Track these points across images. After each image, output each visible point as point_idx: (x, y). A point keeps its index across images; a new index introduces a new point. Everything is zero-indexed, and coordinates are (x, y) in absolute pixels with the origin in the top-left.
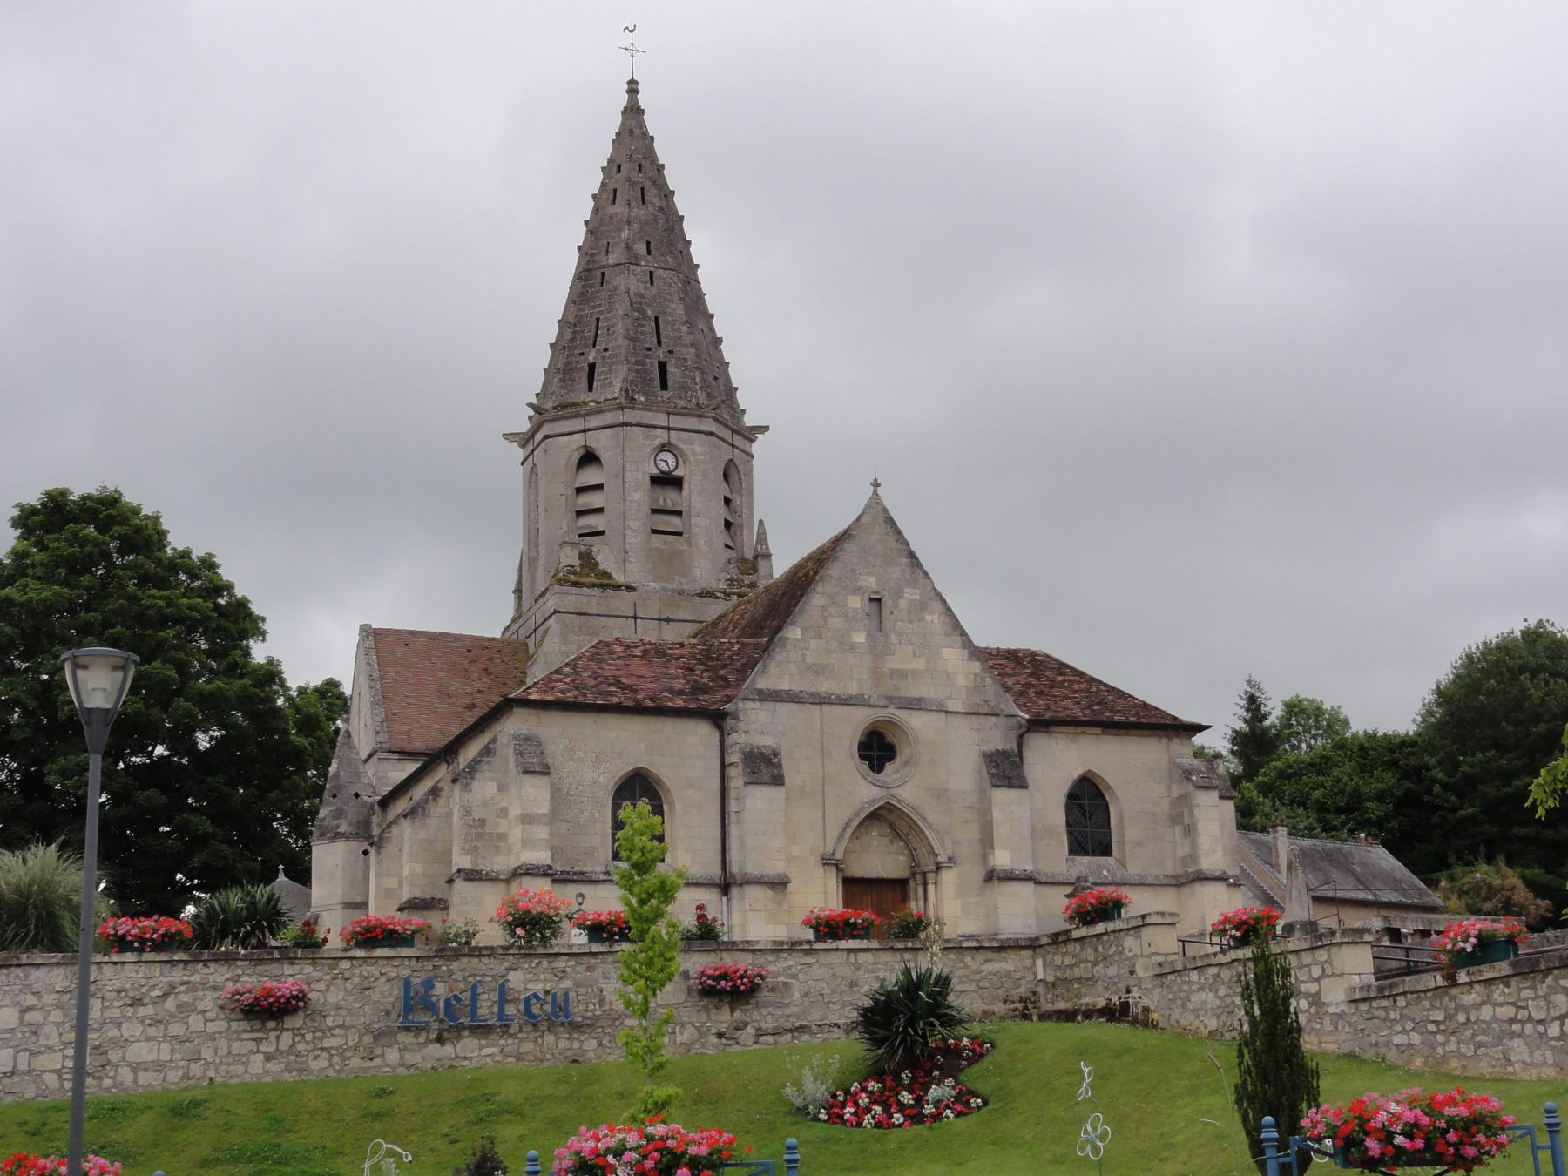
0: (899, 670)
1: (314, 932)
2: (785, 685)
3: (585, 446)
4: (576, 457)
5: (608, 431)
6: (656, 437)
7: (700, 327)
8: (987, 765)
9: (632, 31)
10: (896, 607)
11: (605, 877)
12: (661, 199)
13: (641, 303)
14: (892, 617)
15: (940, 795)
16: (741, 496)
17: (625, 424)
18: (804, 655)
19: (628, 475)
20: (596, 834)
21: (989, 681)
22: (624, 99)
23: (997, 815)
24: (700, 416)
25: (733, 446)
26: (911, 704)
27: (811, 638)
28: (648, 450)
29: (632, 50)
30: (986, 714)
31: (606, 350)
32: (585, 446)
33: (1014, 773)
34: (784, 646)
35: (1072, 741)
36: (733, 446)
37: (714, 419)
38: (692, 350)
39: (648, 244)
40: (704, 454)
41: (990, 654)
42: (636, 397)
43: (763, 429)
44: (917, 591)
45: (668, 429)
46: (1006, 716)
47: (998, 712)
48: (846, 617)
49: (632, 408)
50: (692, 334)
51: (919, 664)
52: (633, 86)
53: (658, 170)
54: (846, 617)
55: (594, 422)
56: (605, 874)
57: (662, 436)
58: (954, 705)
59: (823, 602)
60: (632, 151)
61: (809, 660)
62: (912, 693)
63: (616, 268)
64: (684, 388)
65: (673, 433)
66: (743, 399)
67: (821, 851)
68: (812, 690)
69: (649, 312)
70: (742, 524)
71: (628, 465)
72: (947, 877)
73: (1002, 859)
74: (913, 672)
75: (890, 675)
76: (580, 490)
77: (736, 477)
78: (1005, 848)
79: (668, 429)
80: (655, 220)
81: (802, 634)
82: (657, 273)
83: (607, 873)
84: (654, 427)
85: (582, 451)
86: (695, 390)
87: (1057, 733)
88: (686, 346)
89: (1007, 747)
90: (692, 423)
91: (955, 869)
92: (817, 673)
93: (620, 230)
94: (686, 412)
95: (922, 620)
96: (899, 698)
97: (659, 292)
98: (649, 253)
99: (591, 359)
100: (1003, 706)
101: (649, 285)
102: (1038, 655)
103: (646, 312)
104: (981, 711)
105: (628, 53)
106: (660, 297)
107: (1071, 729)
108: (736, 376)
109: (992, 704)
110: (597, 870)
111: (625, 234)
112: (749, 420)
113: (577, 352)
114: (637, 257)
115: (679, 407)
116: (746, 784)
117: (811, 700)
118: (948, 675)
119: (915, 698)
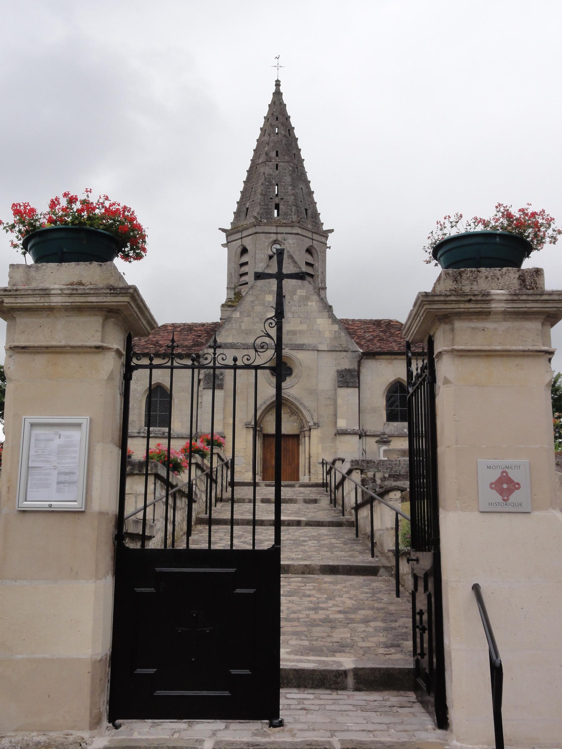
0: (292, 331)
1: (139, 462)
2: (230, 340)
3: (242, 245)
4: (239, 250)
5: (250, 237)
6: (271, 238)
7: (300, 186)
8: (338, 376)
9: (278, 58)
10: (292, 299)
11: (137, 435)
12: (286, 131)
13: (270, 179)
14: (290, 305)
15: (312, 392)
16: (318, 262)
17: (256, 233)
18: (240, 326)
19: (257, 256)
20: (135, 414)
21: (343, 334)
22: (273, 89)
23: (339, 401)
24: (292, 226)
25: (312, 239)
26: (298, 347)
27: (245, 316)
28: (267, 244)
29: (278, 67)
30: (341, 351)
31: (253, 201)
32: (242, 245)
33: (352, 380)
34: (230, 321)
35: (389, 363)
36: (312, 239)
37: (299, 227)
38: (292, 197)
39: (277, 152)
40: (294, 244)
41: (365, 322)
42: (262, 220)
43: (331, 231)
44: (304, 291)
45: (277, 233)
46: (352, 351)
47: (347, 349)
48: (264, 306)
49: (260, 225)
50: (294, 190)
51: (304, 327)
52: (278, 83)
53: (287, 119)
54: (264, 306)
55: (245, 233)
56: (138, 433)
57: (274, 237)
58: (321, 347)
59: (252, 299)
60: (274, 112)
61: (243, 328)
62: (299, 342)
63: (262, 165)
64: (286, 214)
65: (279, 235)
66: (322, 218)
67: (246, 421)
68: (244, 342)
69: (274, 182)
70: (318, 275)
71: (257, 252)
72: (314, 433)
73: (342, 424)
74: (300, 331)
75: (287, 333)
76: (242, 265)
77: (316, 255)
78: (343, 418)
79: (277, 233)
80: (282, 141)
81: (240, 315)
82: (280, 164)
83: (139, 433)
84: (270, 233)
85: (241, 247)
86: (291, 215)
87: (381, 359)
88: (290, 196)
89: (352, 367)
90: (289, 230)
91: (319, 429)
92: (247, 334)
93: (265, 147)
94: (285, 225)
95: (306, 305)
96: (291, 344)
97: (280, 173)
98: (277, 155)
99: (247, 206)
100: (350, 347)
101: (275, 170)
102: (392, 322)
103: (272, 182)
104: (337, 349)
105: (276, 68)
106: (280, 174)
107: (389, 357)
108: (320, 208)
109: (344, 346)
110: (135, 431)
111: (266, 149)
112: (325, 228)
113: (243, 203)
114: (271, 158)
115: (282, 222)
116: (204, 389)
117: (243, 347)
118: (320, 332)
119: (300, 344)
